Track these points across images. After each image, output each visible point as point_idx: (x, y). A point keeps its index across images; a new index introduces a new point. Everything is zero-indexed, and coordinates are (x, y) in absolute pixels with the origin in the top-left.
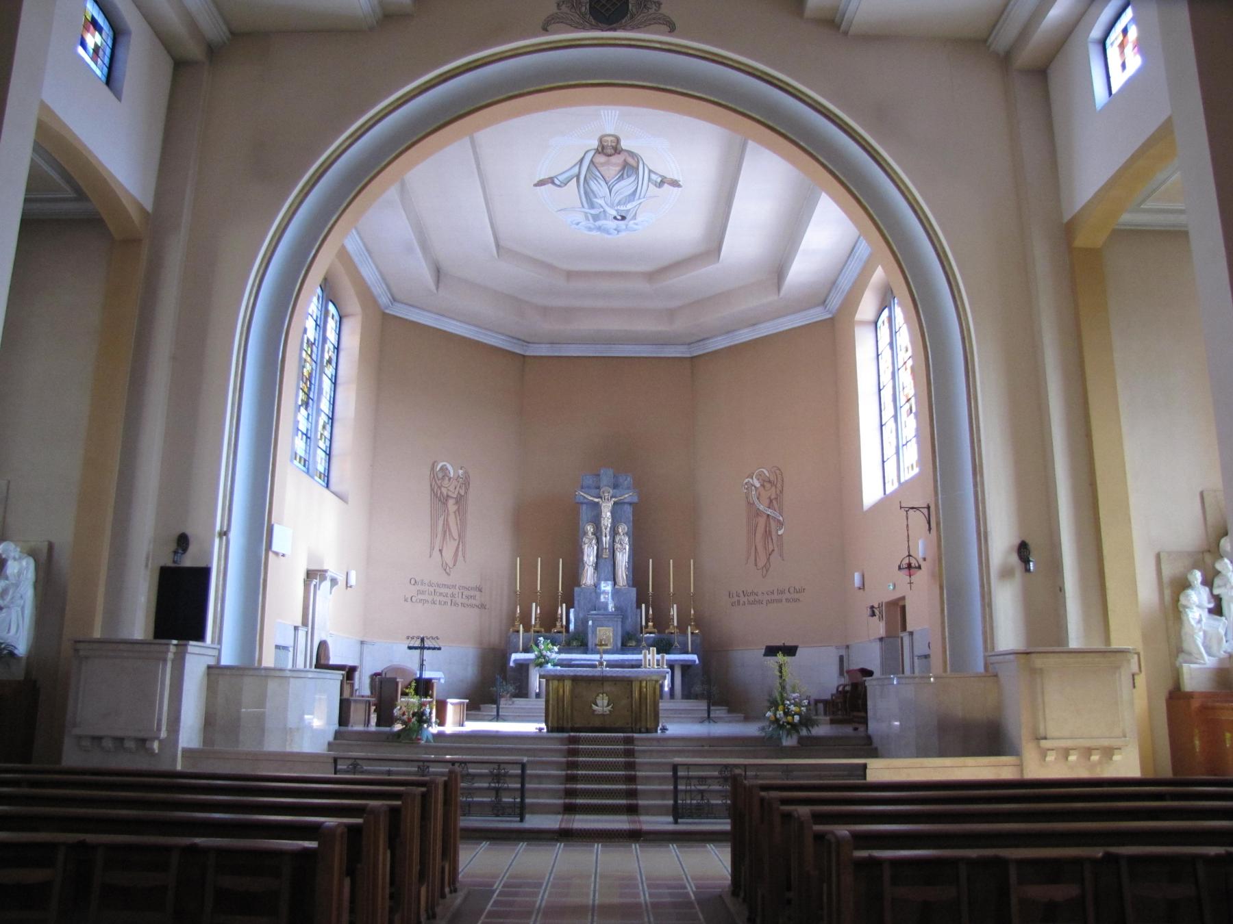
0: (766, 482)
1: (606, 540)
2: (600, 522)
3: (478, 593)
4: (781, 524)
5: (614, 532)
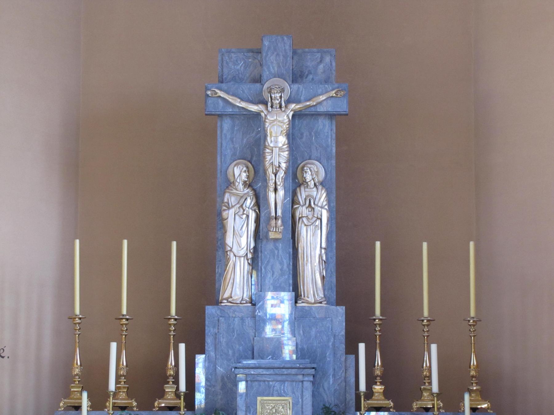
1: (276, 198)
2: (261, 157)
5: (295, 181)
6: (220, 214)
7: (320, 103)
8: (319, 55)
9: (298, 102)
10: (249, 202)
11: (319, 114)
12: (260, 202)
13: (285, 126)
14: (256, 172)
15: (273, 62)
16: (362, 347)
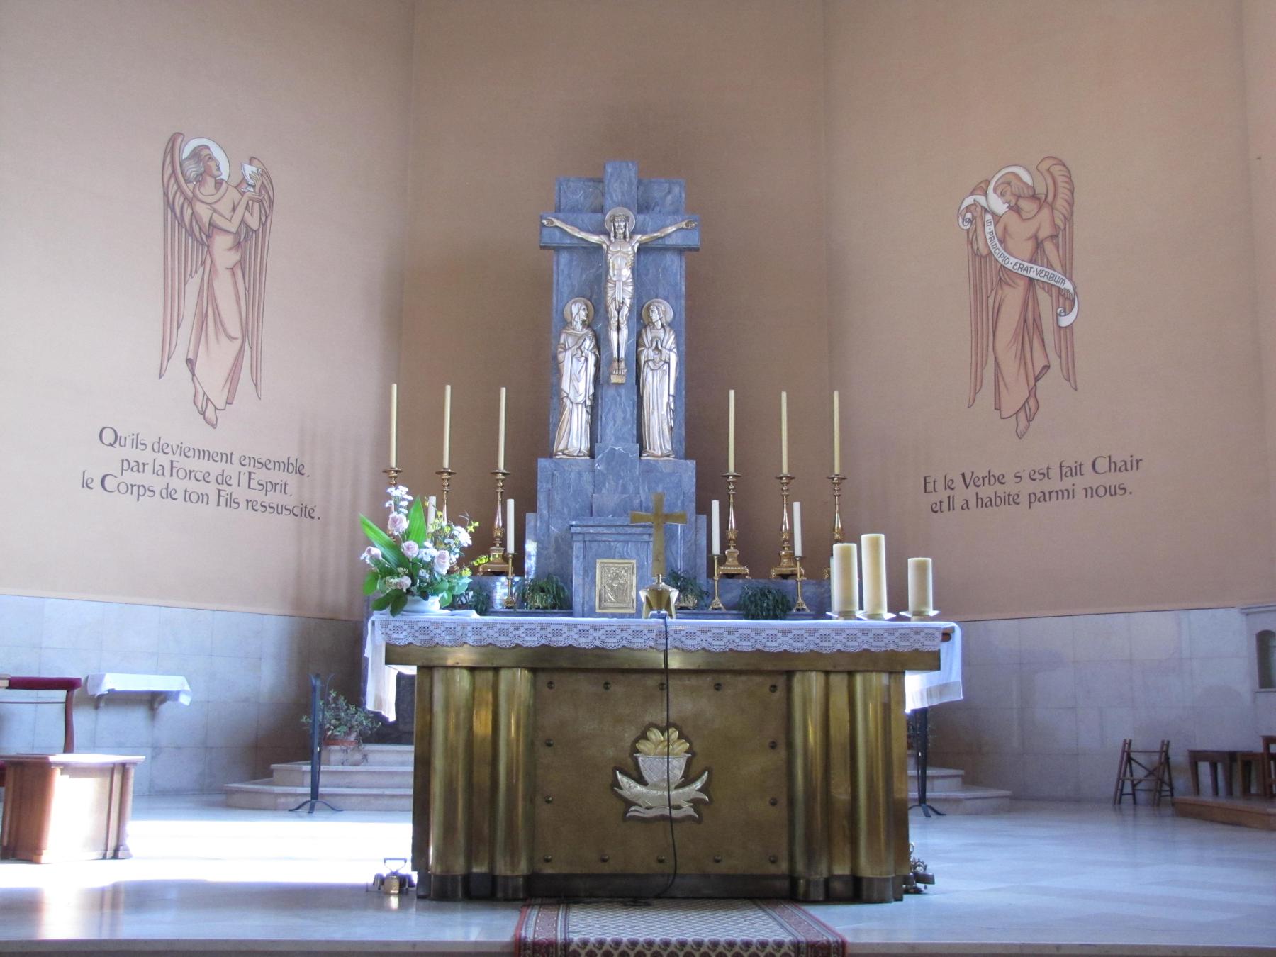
0: (1020, 197)
1: (619, 339)
2: (602, 293)
3: (292, 479)
4: (1066, 300)
5: (640, 321)
6: (555, 357)
7: (669, 235)
8: (667, 185)
9: (644, 233)
10: (588, 344)
11: (666, 249)
12: (600, 343)
13: (631, 258)
14: (596, 312)
15: (616, 189)
16: (715, 505)
